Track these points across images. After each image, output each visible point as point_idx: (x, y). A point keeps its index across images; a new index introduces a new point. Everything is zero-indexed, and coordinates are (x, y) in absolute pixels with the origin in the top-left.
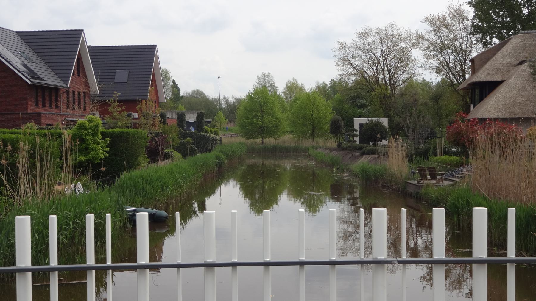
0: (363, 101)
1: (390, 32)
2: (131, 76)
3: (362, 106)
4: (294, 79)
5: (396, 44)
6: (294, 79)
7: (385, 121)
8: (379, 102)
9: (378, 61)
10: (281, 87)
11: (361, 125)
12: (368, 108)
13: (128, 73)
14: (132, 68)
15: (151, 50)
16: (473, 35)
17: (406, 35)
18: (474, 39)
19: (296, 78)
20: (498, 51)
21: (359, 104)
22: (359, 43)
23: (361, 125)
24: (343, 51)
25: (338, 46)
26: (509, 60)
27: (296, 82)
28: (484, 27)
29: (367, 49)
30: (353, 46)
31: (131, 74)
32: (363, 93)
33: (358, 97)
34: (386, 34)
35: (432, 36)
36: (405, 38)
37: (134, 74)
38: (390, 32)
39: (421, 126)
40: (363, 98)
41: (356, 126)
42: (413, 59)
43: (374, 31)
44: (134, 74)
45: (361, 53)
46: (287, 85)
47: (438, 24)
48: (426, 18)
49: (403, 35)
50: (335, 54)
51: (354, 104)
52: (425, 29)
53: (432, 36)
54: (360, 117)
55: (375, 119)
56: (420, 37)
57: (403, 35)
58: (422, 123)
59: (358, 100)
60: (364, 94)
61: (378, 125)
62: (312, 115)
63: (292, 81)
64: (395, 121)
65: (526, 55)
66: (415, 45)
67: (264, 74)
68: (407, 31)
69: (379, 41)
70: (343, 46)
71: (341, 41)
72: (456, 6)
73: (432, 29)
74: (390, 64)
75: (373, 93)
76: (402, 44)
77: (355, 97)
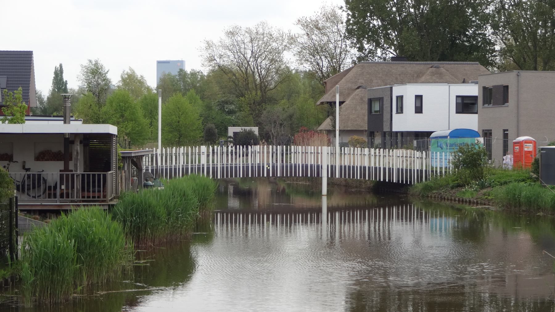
0: (232, 107)
1: (261, 31)
2: (9, 85)
3: (231, 112)
4: (131, 69)
5: (266, 44)
6: (131, 69)
7: (256, 130)
8: (249, 109)
9: (248, 62)
10: (115, 80)
11: (235, 134)
12: (237, 114)
13: (6, 79)
14: (10, 73)
15: (27, 56)
16: (348, 38)
17: (278, 35)
18: (348, 42)
19: (133, 68)
20: (345, 76)
21: (227, 110)
22: (228, 41)
23: (235, 134)
24: (210, 51)
25: (204, 45)
26: (350, 85)
27: (134, 72)
28: (358, 31)
29: (235, 48)
30: (220, 44)
31: (10, 79)
32: (232, 98)
33: (226, 102)
34: (257, 33)
35: (304, 39)
36: (277, 38)
37: (12, 79)
38: (261, 31)
39: (282, 135)
40: (232, 103)
41: (230, 134)
42: (284, 62)
43: (243, 29)
44: (12, 79)
45: (229, 53)
46: (122, 77)
47: (312, 27)
48: (299, 21)
49: (275, 34)
50: (201, 53)
51: (222, 109)
52: (298, 31)
53: (304, 39)
54: (234, 126)
55: (248, 128)
56: (293, 40)
57: (275, 35)
58: (283, 133)
59: (226, 106)
60: (233, 99)
61: (251, 133)
62: (179, 122)
63: (129, 72)
64: (265, 130)
65: (363, 81)
66: (286, 48)
67: (90, 61)
68: (279, 30)
69: (248, 39)
70: (209, 45)
71: (207, 40)
72: (329, 10)
73: (304, 32)
74: (260, 66)
75: (243, 99)
76: (274, 45)
77: (223, 102)
